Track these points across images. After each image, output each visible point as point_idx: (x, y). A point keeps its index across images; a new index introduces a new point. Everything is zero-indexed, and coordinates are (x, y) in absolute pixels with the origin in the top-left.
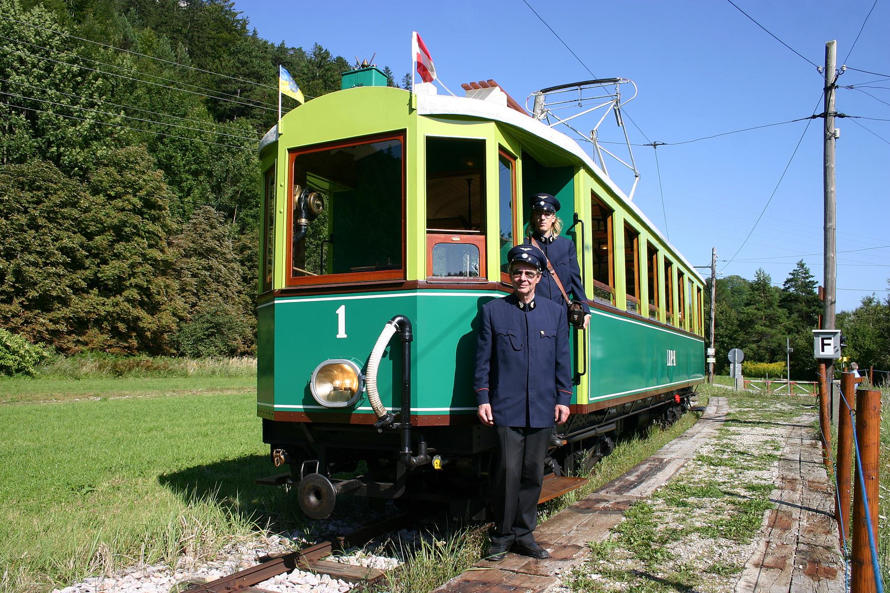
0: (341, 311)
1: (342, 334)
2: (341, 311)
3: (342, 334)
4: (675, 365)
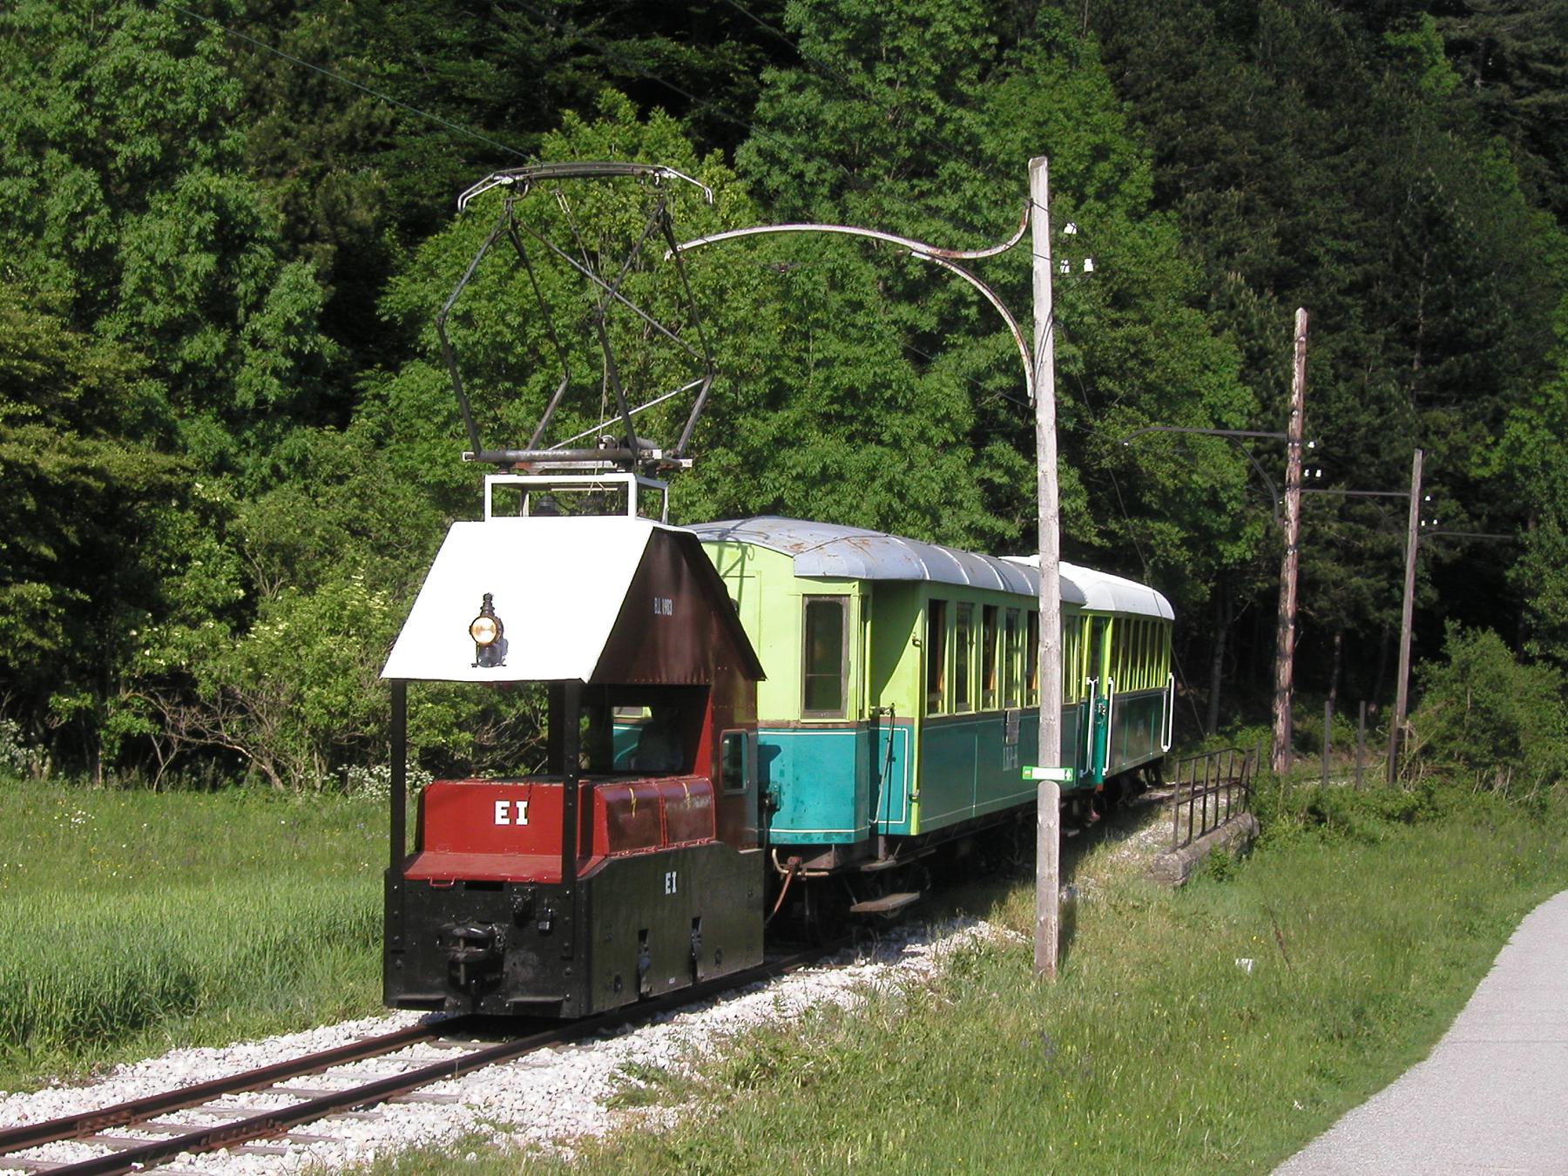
4: (522, 821)
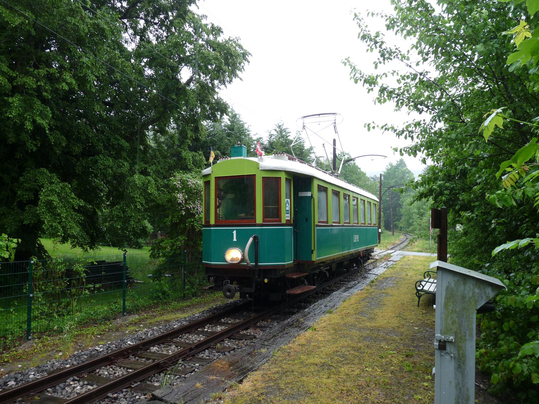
0: (235, 232)
1: (235, 240)
2: (235, 232)
3: (235, 240)
